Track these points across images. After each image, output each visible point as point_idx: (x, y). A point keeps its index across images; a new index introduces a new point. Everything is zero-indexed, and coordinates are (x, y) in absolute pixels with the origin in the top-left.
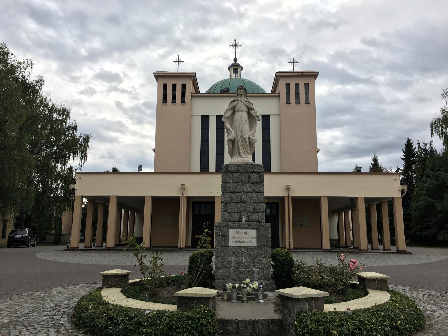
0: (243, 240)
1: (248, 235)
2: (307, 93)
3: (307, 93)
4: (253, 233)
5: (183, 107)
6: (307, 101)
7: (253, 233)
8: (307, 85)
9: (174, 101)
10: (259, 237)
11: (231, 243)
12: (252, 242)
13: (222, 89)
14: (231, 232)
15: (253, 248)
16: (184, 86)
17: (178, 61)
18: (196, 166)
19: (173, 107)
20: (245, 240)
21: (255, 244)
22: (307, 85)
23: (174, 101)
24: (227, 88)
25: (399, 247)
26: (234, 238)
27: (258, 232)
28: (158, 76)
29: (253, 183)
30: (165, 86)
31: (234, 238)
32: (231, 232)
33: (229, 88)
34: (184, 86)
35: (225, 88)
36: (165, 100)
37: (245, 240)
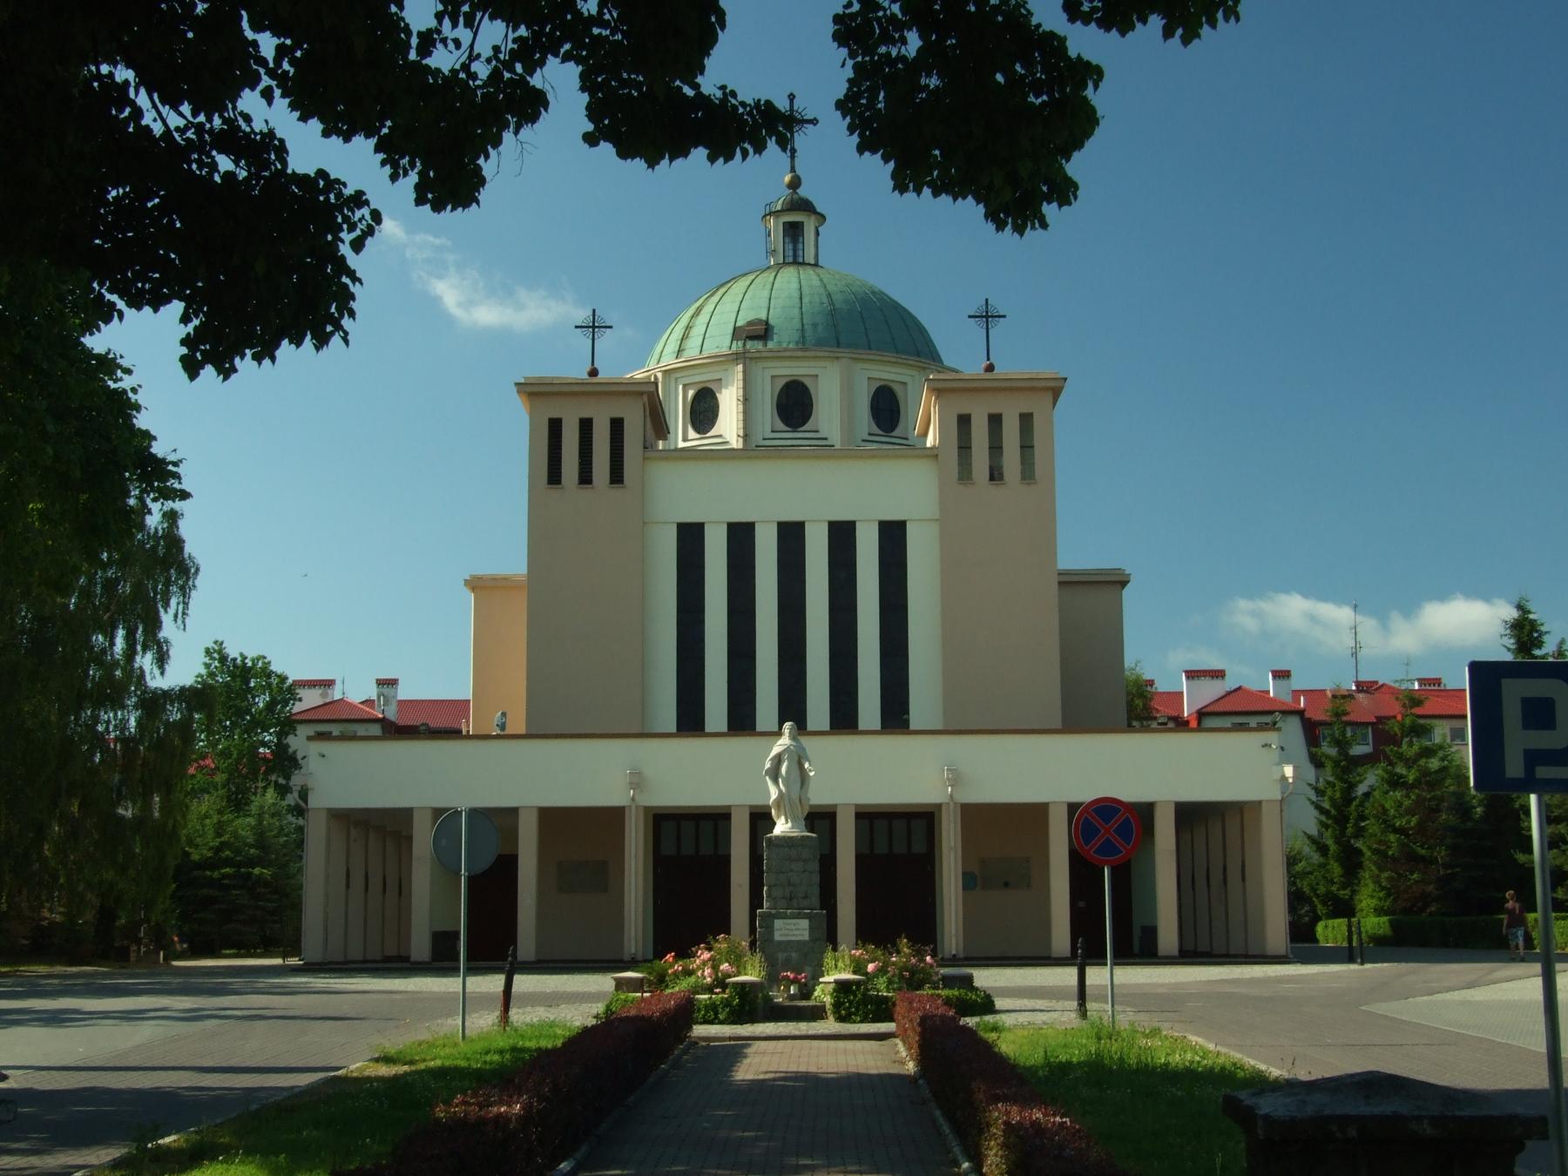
0: (791, 933)
1: (797, 927)
2: (1027, 447)
3: (1027, 447)
4: (805, 923)
5: (616, 493)
6: (1028, 474)
7: (805, 923)
8: (1026, 420)
9: (585, 478)
10: (811, 928)
11: (778, 937)
12: (803, 935)
13: (738, 324)
14: (778, 923)
15: (803, 943)
16: (617, 426)
17: (594, 327)
18: (666, 710)
19: (585, 493)
20: (796, 932)
21: (806, 937)
22: (1026, 420)
23: (585, 478)
24: (759, 321)
25: (413, 916)
26: (781, 929)
27: (810, 921)
28: (534, 391)
29: (804, 861)
30: (555, 426)
31: (781, 929)
32: (778, 923)
33: (767, 323)
34: (617, 426)
35: (750, 323)
36: (554, 477)
37: (796, 932)
